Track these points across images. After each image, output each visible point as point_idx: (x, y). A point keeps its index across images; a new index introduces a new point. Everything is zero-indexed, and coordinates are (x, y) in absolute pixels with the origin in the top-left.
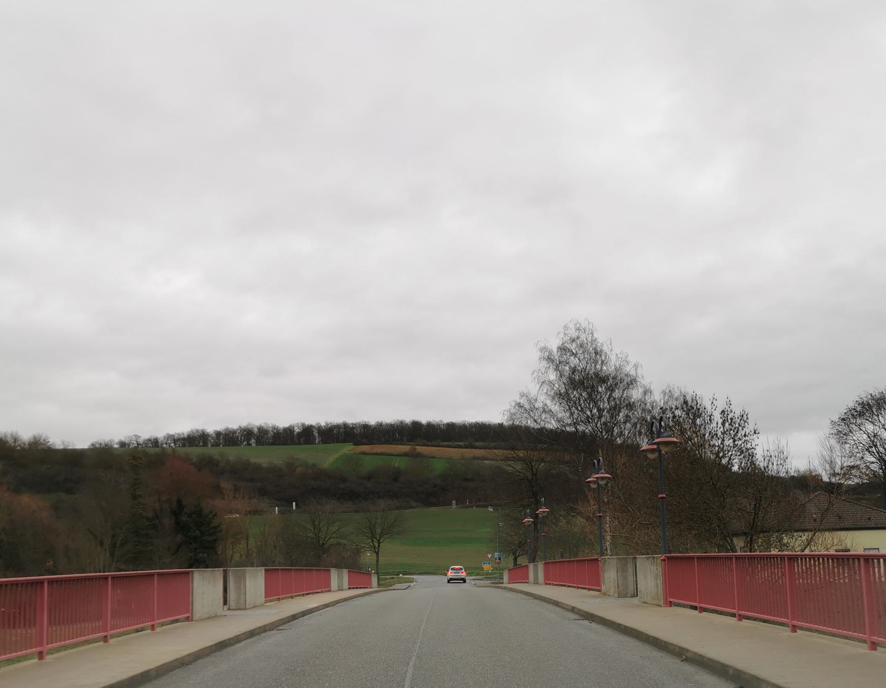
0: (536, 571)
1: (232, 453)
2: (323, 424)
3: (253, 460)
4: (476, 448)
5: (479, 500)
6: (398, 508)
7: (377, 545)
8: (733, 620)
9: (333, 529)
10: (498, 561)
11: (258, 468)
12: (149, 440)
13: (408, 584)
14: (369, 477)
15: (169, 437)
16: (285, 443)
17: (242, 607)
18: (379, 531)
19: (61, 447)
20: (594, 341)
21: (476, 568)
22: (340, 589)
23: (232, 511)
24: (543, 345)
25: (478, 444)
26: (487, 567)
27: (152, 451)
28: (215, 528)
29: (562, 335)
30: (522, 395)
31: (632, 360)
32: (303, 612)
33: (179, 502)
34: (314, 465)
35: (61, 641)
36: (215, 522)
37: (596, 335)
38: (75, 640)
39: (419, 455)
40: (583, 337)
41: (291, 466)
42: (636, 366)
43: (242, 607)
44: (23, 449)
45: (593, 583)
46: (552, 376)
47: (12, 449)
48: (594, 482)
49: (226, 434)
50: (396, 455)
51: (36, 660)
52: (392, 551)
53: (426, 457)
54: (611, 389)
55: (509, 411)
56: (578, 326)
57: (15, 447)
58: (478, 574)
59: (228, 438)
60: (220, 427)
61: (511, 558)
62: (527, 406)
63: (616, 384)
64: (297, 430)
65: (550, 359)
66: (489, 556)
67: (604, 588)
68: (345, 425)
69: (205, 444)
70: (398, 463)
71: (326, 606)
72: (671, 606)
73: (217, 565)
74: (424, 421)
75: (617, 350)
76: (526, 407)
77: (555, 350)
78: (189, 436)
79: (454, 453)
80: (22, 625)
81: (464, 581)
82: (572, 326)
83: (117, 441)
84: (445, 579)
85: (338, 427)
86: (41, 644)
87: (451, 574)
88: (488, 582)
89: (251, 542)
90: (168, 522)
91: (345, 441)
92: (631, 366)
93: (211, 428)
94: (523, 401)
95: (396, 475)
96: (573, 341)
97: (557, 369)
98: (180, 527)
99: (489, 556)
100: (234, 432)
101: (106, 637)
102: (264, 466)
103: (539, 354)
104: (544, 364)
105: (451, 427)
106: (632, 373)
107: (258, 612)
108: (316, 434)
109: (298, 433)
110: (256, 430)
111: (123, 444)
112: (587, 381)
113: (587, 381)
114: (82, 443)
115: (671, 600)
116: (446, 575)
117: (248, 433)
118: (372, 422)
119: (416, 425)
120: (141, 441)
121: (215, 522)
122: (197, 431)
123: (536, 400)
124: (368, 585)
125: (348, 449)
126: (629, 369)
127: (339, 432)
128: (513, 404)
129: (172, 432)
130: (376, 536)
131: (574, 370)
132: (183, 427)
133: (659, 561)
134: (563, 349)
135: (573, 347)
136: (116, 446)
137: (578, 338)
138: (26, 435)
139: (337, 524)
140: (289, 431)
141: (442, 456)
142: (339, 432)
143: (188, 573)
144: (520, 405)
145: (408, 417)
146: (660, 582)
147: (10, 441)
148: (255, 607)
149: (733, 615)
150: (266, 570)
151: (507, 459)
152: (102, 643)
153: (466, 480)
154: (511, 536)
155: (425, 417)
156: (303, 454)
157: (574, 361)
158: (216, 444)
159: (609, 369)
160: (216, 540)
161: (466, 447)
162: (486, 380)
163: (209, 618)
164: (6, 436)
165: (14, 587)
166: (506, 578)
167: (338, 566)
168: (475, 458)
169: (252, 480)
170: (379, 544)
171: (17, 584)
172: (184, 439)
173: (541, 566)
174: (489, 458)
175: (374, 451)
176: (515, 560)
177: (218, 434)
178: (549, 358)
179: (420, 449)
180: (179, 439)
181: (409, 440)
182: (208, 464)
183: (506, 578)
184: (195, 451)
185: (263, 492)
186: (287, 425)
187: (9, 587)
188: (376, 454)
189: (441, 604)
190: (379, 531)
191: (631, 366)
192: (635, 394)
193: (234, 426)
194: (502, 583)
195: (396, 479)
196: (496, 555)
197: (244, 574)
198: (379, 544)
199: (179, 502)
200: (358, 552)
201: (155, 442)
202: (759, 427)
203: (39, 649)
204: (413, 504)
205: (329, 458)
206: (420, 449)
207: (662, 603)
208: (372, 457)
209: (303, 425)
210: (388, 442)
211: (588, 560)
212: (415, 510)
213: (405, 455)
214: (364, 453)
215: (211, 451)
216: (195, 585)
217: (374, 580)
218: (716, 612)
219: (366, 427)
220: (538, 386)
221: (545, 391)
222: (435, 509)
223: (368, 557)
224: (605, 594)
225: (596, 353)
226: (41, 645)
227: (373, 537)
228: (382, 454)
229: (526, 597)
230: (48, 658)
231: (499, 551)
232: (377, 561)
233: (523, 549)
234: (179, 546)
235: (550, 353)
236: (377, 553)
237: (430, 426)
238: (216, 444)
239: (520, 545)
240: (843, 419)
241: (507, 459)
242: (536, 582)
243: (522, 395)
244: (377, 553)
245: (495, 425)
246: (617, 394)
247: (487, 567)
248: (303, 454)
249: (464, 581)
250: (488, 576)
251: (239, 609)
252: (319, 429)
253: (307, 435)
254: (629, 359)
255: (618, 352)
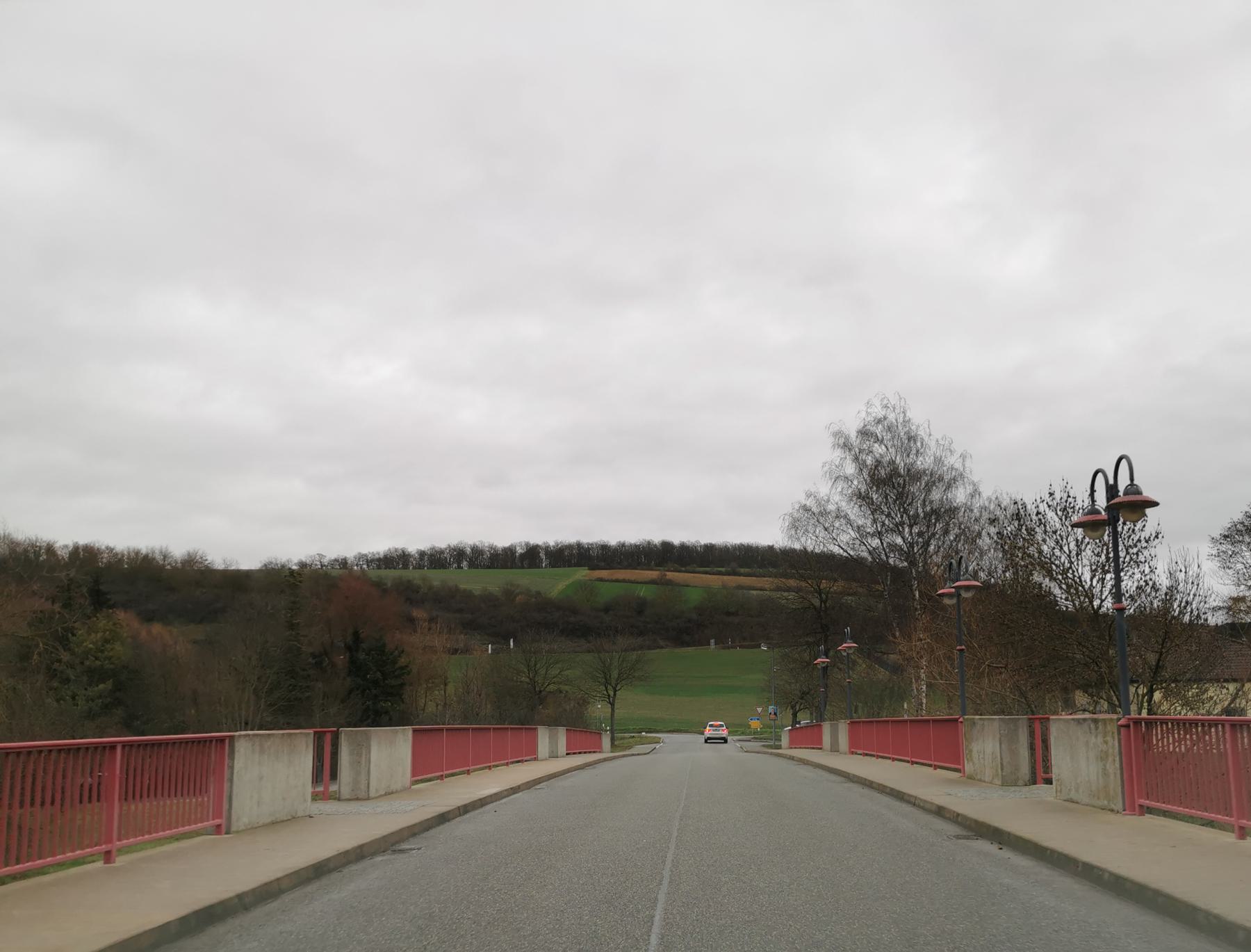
0: (837, 732)
1: (437, 577)
2: (552, 543)
3: (462, 586)
4: (740, 575)
5: (744, 639)
6: (641, 648)
7: (612, 693)
8: (931, 770)
9: (554, 672)
10: (773, 716)
11: (468, 595)
12: (336, 560)
13: (653, 746)
14: (607, 609)
15: (361, 557)
16: (504, 567)
17: (361, 796)
18: (615, 674)
19: (221, 567)
20: (907, 422)
21: (740, 725)
22: (554, 755)
23: (424, 646)
24: (836, 429)
25: (742, 570)
26: (755, 724)
27: (336, 572)
28: (402, 668)
29: (863, 414)
30: (809, 495)
31: (959, 448)
32: (465, 806)
33: (356, 635)
34: (539, 593)
35: (177, 827)
36: (403, 661)
37: (908, 414)
38: (193, 827)
39: (669, 583)
40: (892, 417)
41: (509, 594)
42: (963, 457)
43: (362, 794)
44: (175, 569)
45: (817, 744)
46: (850, 469)
47: (162, 568)
48: (950, 595)
49: (431, 555)
50: (645, 583)
51: (100, 864)
52: (632, 702)
53: (678, 585)
54: (928, 488)
55: (791, 515)
56: (885, 402)
57: (164, 566)
58: (743, 733)
59: (434, 559)
60: (424, 546)
61: (790, 712)
62: (815, 509)
63: (934, 482)
64: (519, 551)
65: (846, 446)
66: (759, 710)
67: (968, 768)
68: (579, 545)
69: (406, 566)
70: (643, 591)
71: (514, 790)
72: (1142, 814)
73: (402, 721)
74: (676, 541)
75: (937, 435)
76: (812, 515)
77: (853, 435)
78: (385, 557)
79: (714, 581)
80: (179, 793)
81: (726, 741)
82: (877, 403)
83: (296, 561)
84: (702, 739)
85: (570, 547)
86: (109, 840)
87: (709, 732)
88: (756, 745)
89: (451, 689)
90: (341, 659)
91: (578, 565)
92: (957, 455)
93: (414, 545)
94: (810, 503)
95: (641, 607)
96: (879, 421)
97: (856, 459)
98: (355, 668)
99: (759, 710)
100: (442, 552)
101: (219, 826)
102: (477, 593)
103: (832, 439)
104: (839, 453)
105: (710, 548)
106: (958, 465)
107: (384, 805)
108: (542, 555)
109: (521, 555)
110: (469, 549)
111: (303, 565)
112: (895, 480)
113: (895, 480)
114: (249, 562)
115: (1142, 801)
116: (702, 733)
117: (459, 554)
118: (613, 541)
119: (667, 546)
120: (325, 561)
121: (403, 661)
122: (396, 550)
123: (828, 501)
124: (598, 748)
125: (582, 574)
126: (953, 460)
127: (572, 555)
128: (797, 507)
129: (365, 551)
130: (610, 684)
131: (878, 463)
132: (379, 546)
133: (1112, 728)
134: (864, 433)
135: (879, 430)
136: (294, 567)
137: (885, 418)
138: (178, 551)
139: (559, 665)
140: (509, 552)
141: (699, 585)
142: (572, 555)
143: (221, 740)
144: (806, 509)
145: (657, 538)
146: (1113, 767)
147: (158, 557)
148: (389, 794)
149: (930, 766)
150: (414, 731)
151: (778, 589)
152: (100, 864)
153: (729, 614)
154: (790, 684)
155: (677, 538)
156: (524, 579)
157: (879, 449)
158: (420, 567)
159: (924, 462)
160: (402, 685)
161: (728, 574)
162: (756, 486)
163: (273, 823)
164: (153, 552)
165: (63, 755)
166: (785, 741)
167: (553, 722)
168: (740, 587)
169: (460, 611)
170: (615, 691)
171: (18, 754)
172: (379, 560)
173: (843, 728)
174: (759, 585)
175: (614, 578)
176: (795, 715)
177: (422, 554)
178: (845, 445)
179: (670, 575)
180: (372, 561)
181: (657, 565)
182: (409, 593)
183: (785, 741)
184: (390, 575)
185: (471, 626)
186: (507, 545)
187: (54, 754)
188: (617, 581)
189: (695, 778)
190: (615, 674)
191: (957, 455)
192: (960, 496)
193: (442, 544)
194: (779, 747)
195: (640, 612)
196: (771, 709)
197: (368, 739)
198: (615, 691)
199: (356, 635)
200: (583, 703)
201: (344, 563)
202: (1164, 529)
203: (104, 847)
204: (662, 643)
205: (557, 583)
206: (670, 575)
207: (1119, 806)
208: (612, 584)
209: (527, 544)
210: (630, 567)
211: (934, 721)
212: (664, 651)
213: (653, 582)
214: (601, 580)
215: (411, 574)
216: (239, 763)
217: (606, 741)
218: (1165, 814)
219: (604, 547)
220: (830, 484)
221: (839, 489)
222: (690, 649)
223: (599, 709)
224: (971, 777)
225: (909, 439)
226: (109, 841)
227: (607, 683)
228: (624, 581)
229: (866, 791)
230: (120, 861)
231: (776, 704)
232: (612, 715)
233: (806, 702)
234: (350, 692)
235: (847, 438)
236: (612, 705)
237: (683, 547)
238: (420, 567)
239: (804, 695)
240: (1226, 537)
241: (778, 589)
242: (835, 749)
243: (809, 495)
244: (612, 705)
245: (764, 548)
246: (936, 495)
247: (755, 724)
248: (524, 579)
249: (725, 740)
250: (757, 736)
251: (357, 799)
252: (547, 549)
253: (531, 556)
254: (954, 446)
255: (940, 437)
